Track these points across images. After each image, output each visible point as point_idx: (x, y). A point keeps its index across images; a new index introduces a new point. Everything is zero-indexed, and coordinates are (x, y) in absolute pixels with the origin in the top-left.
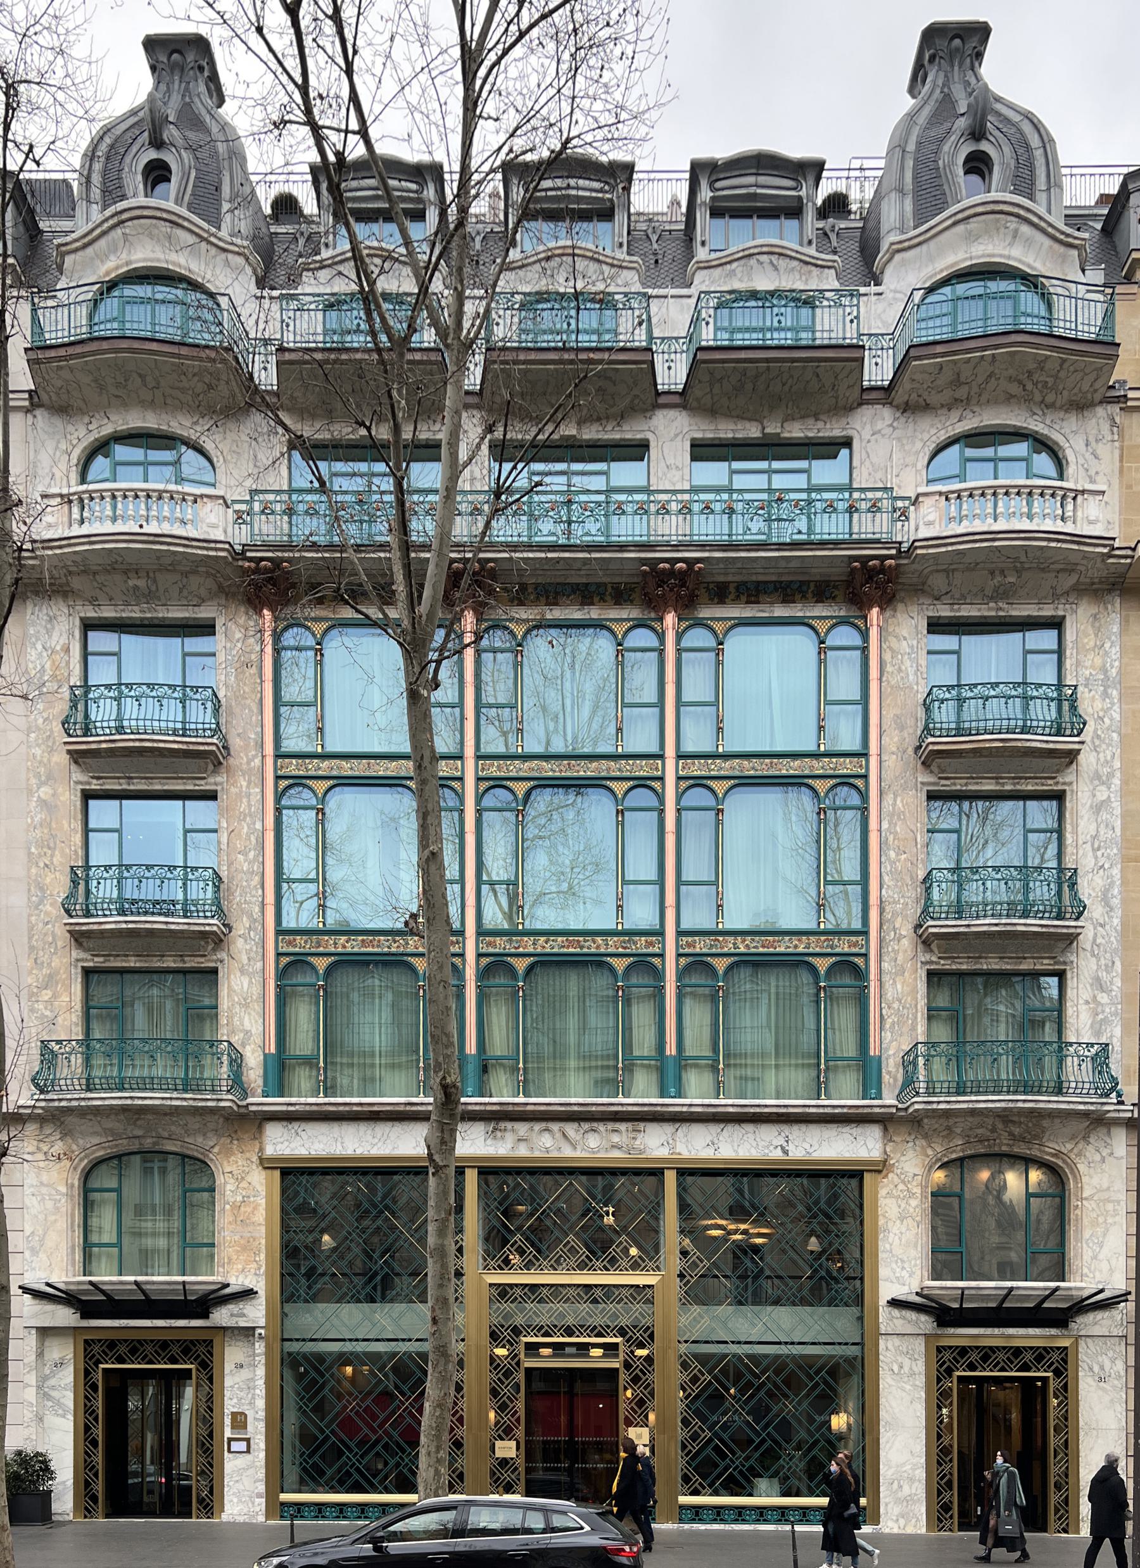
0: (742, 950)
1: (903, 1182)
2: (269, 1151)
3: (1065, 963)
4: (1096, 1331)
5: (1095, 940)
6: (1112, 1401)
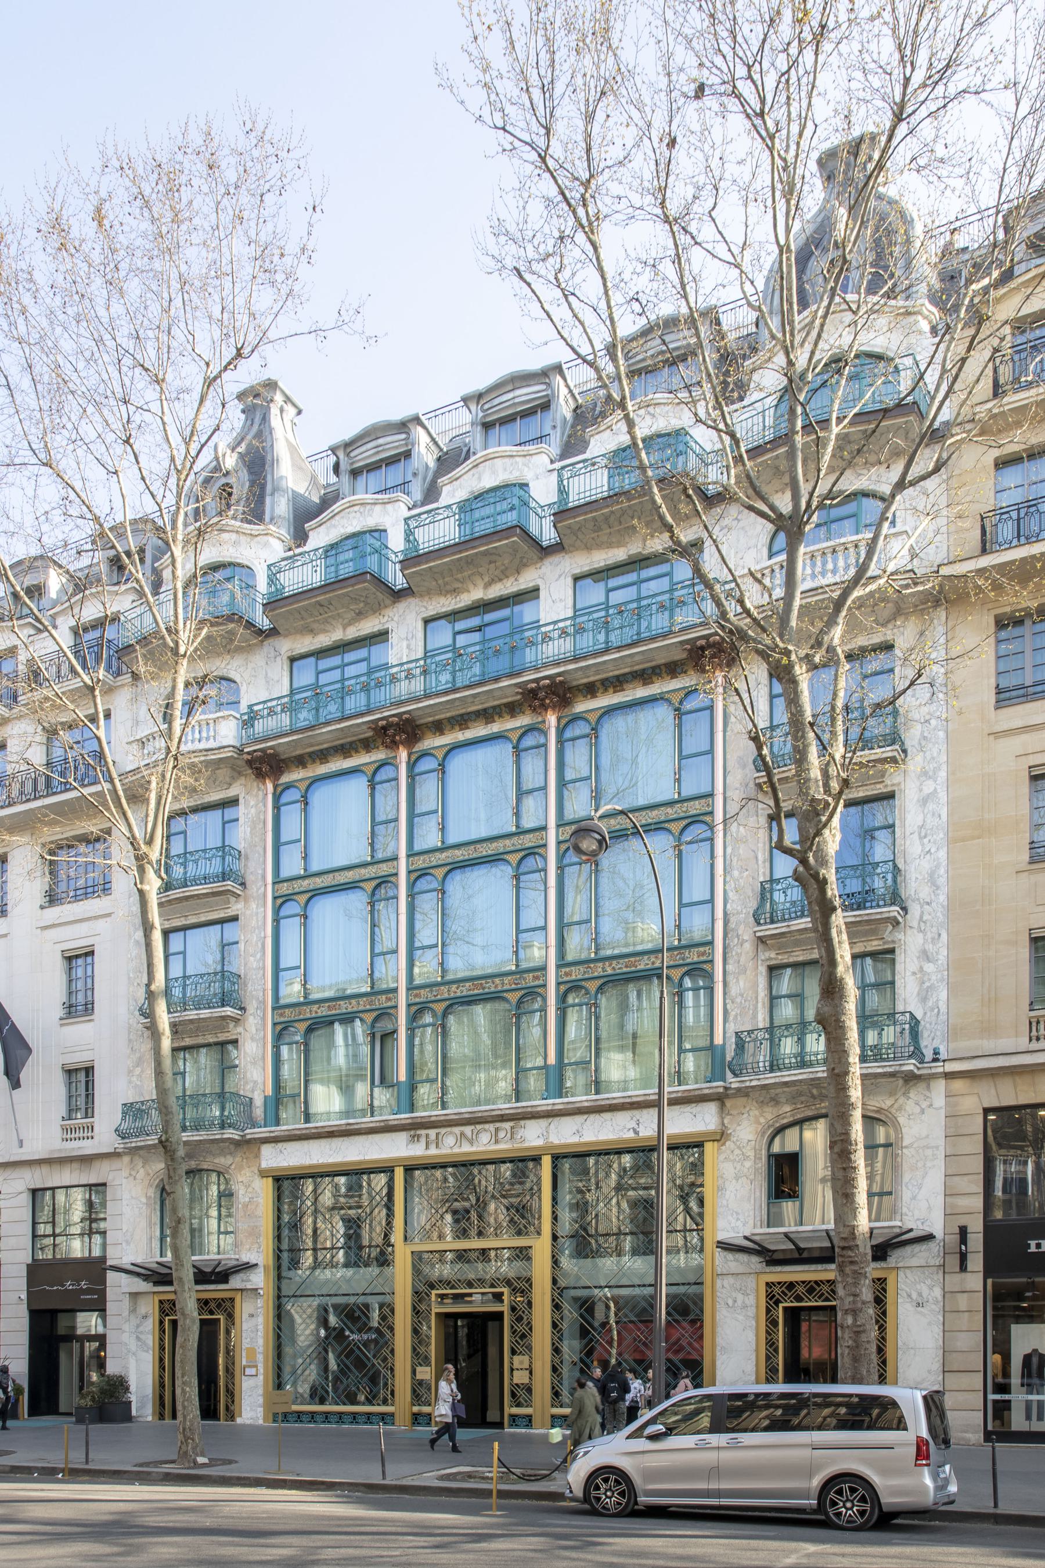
0: (610, 971)
1: (739, 1148)
2: (264, 1165)
3: (893, 942)
4: (914, 1262)
5: (921, 917)
6: (930, 1324)
